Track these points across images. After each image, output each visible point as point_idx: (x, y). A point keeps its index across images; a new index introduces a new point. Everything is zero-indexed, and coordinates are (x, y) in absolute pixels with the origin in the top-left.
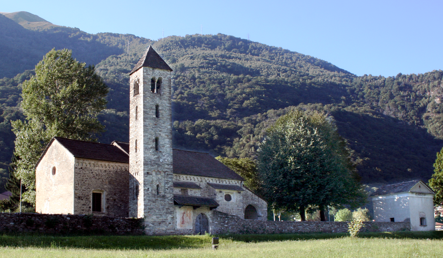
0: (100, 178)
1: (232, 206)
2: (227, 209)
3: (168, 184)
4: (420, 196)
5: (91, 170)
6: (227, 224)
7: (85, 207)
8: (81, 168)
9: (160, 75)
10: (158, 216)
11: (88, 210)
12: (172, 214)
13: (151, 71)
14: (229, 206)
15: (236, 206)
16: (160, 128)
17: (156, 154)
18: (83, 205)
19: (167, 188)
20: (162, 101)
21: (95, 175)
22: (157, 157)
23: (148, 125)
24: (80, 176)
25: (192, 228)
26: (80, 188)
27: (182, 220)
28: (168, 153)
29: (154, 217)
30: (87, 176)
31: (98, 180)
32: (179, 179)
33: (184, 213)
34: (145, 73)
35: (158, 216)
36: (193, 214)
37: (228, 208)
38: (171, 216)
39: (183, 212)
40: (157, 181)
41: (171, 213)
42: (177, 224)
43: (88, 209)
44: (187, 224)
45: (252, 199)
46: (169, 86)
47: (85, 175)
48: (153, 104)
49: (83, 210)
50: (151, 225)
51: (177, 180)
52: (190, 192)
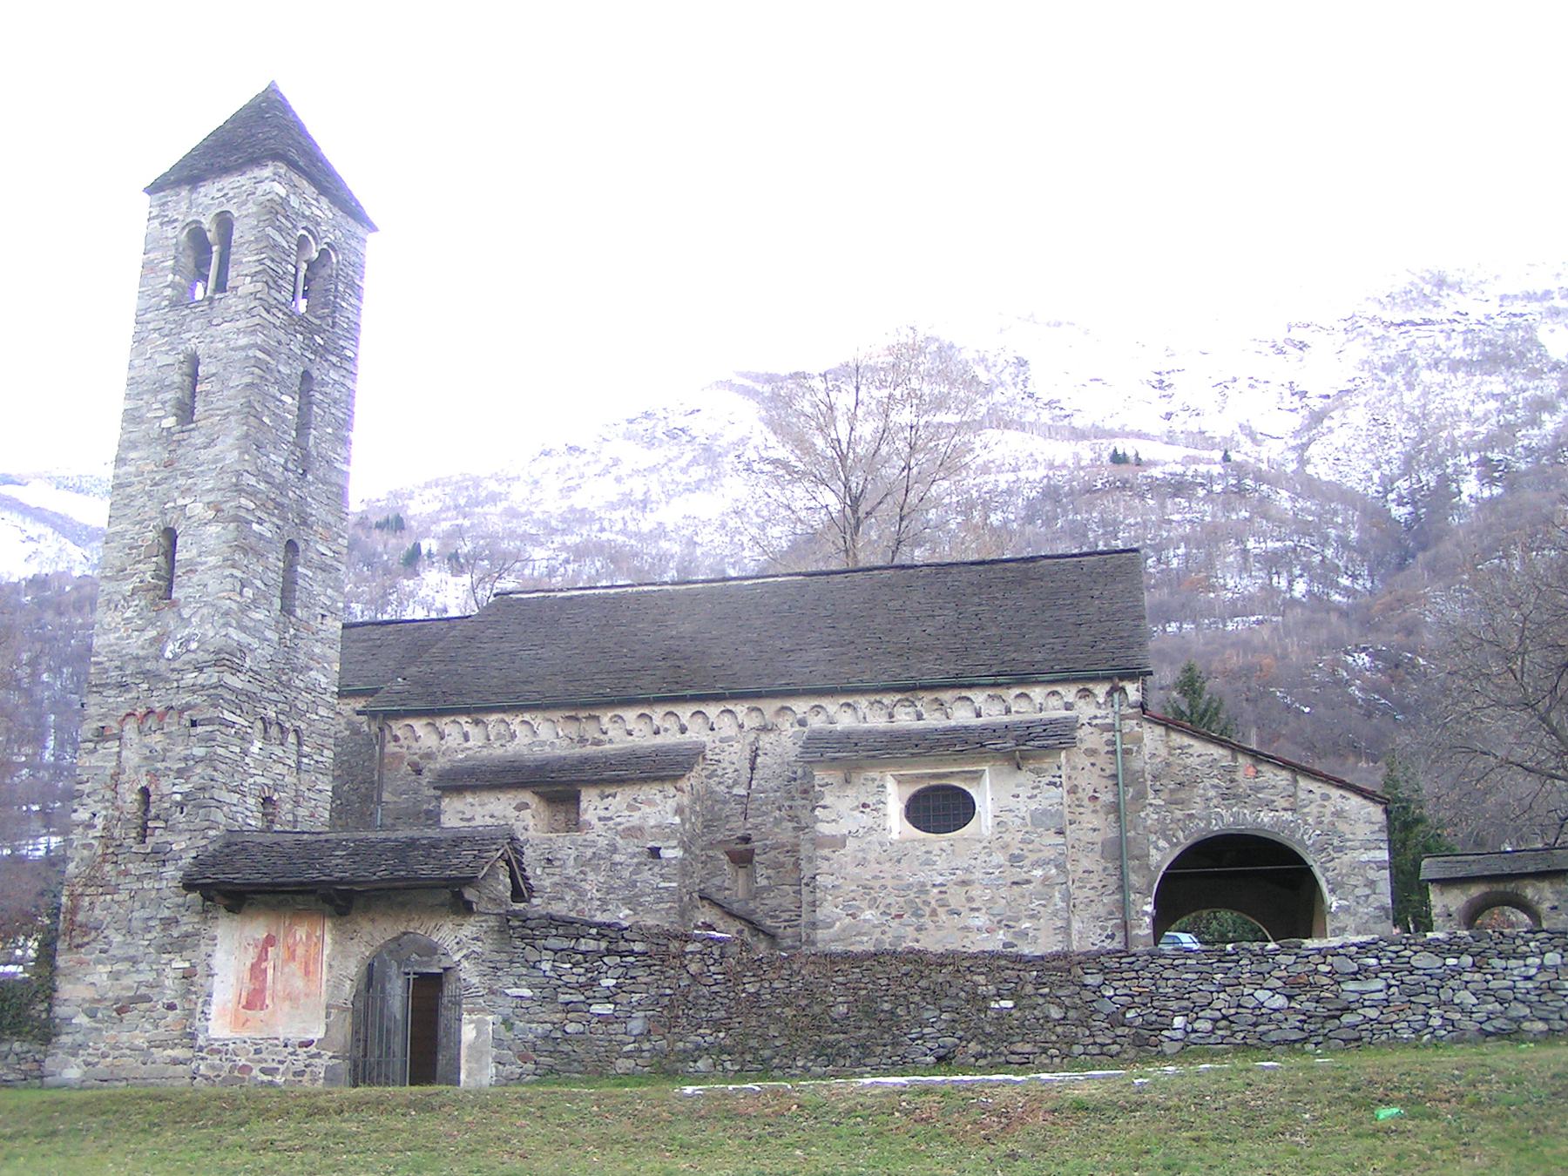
2: (909, 886)
10: (117, 967)
12: (187, 954)
15: (999, 858)
16: (189, 475)
22: (154, 633)
25: (318, 1033)
27: (248, 986)
32: (597, 735)
33: (270, 941)
35: (117, 967)
36: (335, 942)
37: (921, 877)
39: (262, 935)
41: (180, 945)
42: (213, 1011)
44: (286, 1006)
51: (582, 740)
52: (596, 801)
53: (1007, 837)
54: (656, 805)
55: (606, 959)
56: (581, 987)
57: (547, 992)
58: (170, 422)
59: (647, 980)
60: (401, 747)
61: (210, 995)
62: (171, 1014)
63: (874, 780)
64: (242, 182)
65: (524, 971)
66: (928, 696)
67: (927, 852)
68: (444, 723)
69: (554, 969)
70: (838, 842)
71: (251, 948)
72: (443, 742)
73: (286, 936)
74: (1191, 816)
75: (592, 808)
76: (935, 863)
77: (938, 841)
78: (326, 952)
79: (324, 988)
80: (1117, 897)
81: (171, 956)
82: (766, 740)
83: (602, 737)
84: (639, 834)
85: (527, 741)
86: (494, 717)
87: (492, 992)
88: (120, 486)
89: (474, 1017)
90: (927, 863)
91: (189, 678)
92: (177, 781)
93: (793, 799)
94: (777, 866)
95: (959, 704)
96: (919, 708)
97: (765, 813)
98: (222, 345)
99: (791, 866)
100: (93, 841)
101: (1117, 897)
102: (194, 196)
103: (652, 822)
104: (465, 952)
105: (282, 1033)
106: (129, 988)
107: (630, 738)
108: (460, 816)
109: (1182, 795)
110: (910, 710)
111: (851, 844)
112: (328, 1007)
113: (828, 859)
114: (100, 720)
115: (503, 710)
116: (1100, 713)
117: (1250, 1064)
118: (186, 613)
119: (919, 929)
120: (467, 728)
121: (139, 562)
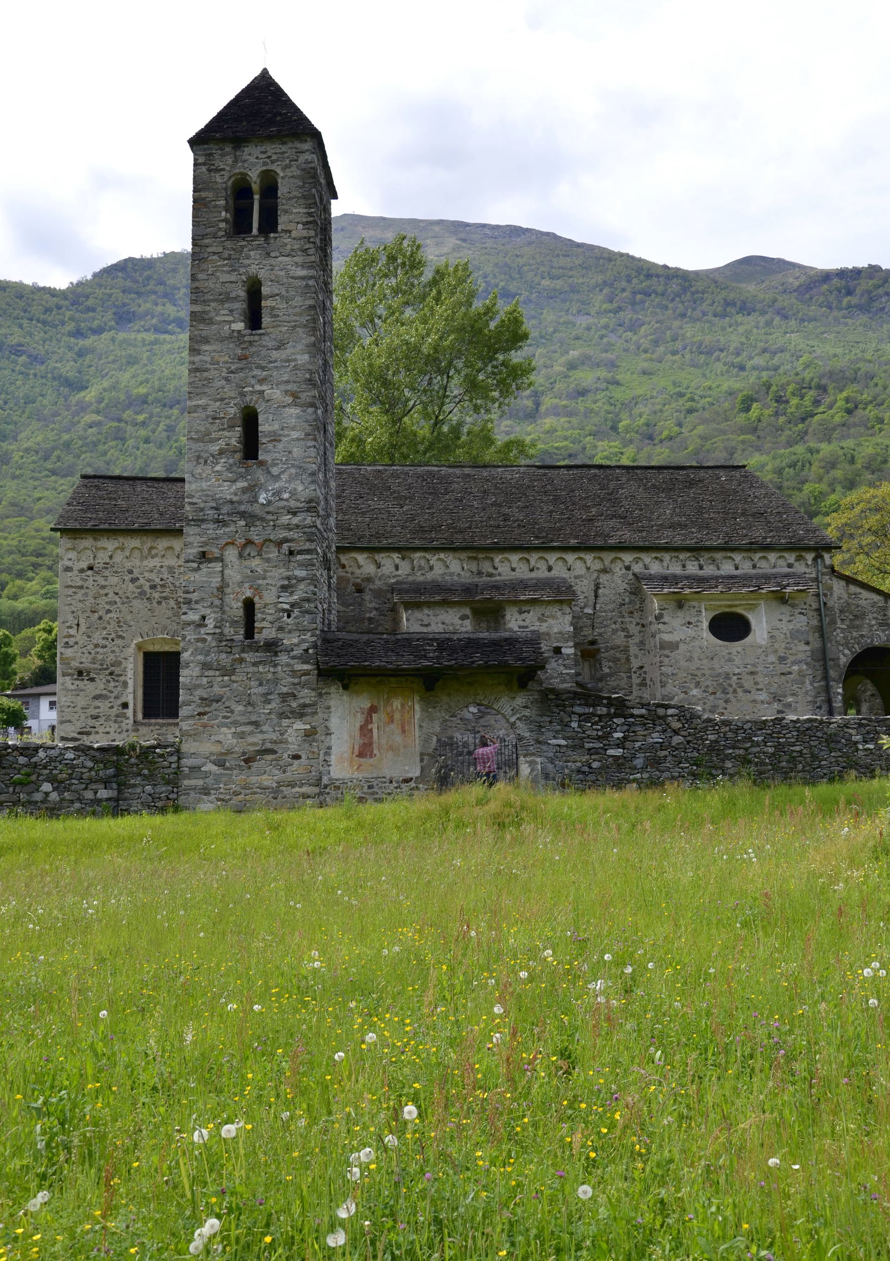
0: (165, 598)
1: (748, 661)
2: (719, 675)
3: (292, 593)
5: (130, 572)
6: (621, 744)
7: (104, 706)
8: (91, 568)
9: (265, 164)
10: (239, 729)
11: (117, 716)
12: (307, 719)
13: (228, 154)
14: (730, 660)
15: (772, 658)
16: (263, 368)
17: (242, 476)
18: (96, 697)
19: (284, 610)
20: (272, 261)
21: (146, 588)
22: (245, 484)
23: (208, 366)
24: (86, 595)
26: (81, 638)
27: (359, 741)
28: (293, 466)
29: (227, 736)
30: (111, 595)
31: (159, 603)
32: (491, 570)
33: (373, 709)
34: (204, 169)
35: (239, 729)
36: (423, 710)
37: (726, 669)
38: (299, 725)
39: (367, 705)
40: (247, 585)
42: (333, 759)
43: (115, 711)
44: (390, 754)
46: (304, 197)
47: (103, 592)
48: (233, 279)
49: (96, 717)
51: (480, 573)
52: (516, 615)
53: (776, 645)
54: (557, 618)
55: (615, 720)
56: (599, 738)
57: (577, 742)
58: (240, 326)
59: (645, 733)
60: (347, 572)
61: (329, 748)
62: (296, 762)
63: (694, 607)
64: (284, 150)
65: (559, 727)
66: (707, 555)
67: (729, 654)
68: (380, 557)
69: (580, 726)
70: (674, 646)
71: (359, 714)
72: (379, 570)
73: (385, 706)
74: (862, 636)
75: (514, 619)
76: (734, 660)
77: (737, 646)
78: (417, 716)
79: (417, 741)
80: (822, 683)
81: (293, 720)
82: (604, 578)
83: (494, 571)
84: (547, 638)
85: (440, 572)
86: (418, 555)
87: (538, 742)
88: (197, 370)
89: (528, 759)
90: (730, 660)
91: (285, 519)
92: (282, 594)
93: (623, 617)
95: (724, 561)
96: (702, 562)
97: (606, 626)
98: (282, 273)
99: (623, 661)
100: (205, 636)
101: (822, 683)
102: (238, 153)
103: (556, 630)
104: (518, 716)
105: (388, 773)
106: (253, 744)
107: (513, 573)
108: (420, 623)
109: (857, 623)
110: (696, 563)
111: (682, 647)
112: (422, 754)
113: (668, 657)
114: (201, 547)
115: (425, 549)
116: (808, 570)
118: (275, 471)
119: (727, 701)
120: (397, 561)
121: (224, 430)
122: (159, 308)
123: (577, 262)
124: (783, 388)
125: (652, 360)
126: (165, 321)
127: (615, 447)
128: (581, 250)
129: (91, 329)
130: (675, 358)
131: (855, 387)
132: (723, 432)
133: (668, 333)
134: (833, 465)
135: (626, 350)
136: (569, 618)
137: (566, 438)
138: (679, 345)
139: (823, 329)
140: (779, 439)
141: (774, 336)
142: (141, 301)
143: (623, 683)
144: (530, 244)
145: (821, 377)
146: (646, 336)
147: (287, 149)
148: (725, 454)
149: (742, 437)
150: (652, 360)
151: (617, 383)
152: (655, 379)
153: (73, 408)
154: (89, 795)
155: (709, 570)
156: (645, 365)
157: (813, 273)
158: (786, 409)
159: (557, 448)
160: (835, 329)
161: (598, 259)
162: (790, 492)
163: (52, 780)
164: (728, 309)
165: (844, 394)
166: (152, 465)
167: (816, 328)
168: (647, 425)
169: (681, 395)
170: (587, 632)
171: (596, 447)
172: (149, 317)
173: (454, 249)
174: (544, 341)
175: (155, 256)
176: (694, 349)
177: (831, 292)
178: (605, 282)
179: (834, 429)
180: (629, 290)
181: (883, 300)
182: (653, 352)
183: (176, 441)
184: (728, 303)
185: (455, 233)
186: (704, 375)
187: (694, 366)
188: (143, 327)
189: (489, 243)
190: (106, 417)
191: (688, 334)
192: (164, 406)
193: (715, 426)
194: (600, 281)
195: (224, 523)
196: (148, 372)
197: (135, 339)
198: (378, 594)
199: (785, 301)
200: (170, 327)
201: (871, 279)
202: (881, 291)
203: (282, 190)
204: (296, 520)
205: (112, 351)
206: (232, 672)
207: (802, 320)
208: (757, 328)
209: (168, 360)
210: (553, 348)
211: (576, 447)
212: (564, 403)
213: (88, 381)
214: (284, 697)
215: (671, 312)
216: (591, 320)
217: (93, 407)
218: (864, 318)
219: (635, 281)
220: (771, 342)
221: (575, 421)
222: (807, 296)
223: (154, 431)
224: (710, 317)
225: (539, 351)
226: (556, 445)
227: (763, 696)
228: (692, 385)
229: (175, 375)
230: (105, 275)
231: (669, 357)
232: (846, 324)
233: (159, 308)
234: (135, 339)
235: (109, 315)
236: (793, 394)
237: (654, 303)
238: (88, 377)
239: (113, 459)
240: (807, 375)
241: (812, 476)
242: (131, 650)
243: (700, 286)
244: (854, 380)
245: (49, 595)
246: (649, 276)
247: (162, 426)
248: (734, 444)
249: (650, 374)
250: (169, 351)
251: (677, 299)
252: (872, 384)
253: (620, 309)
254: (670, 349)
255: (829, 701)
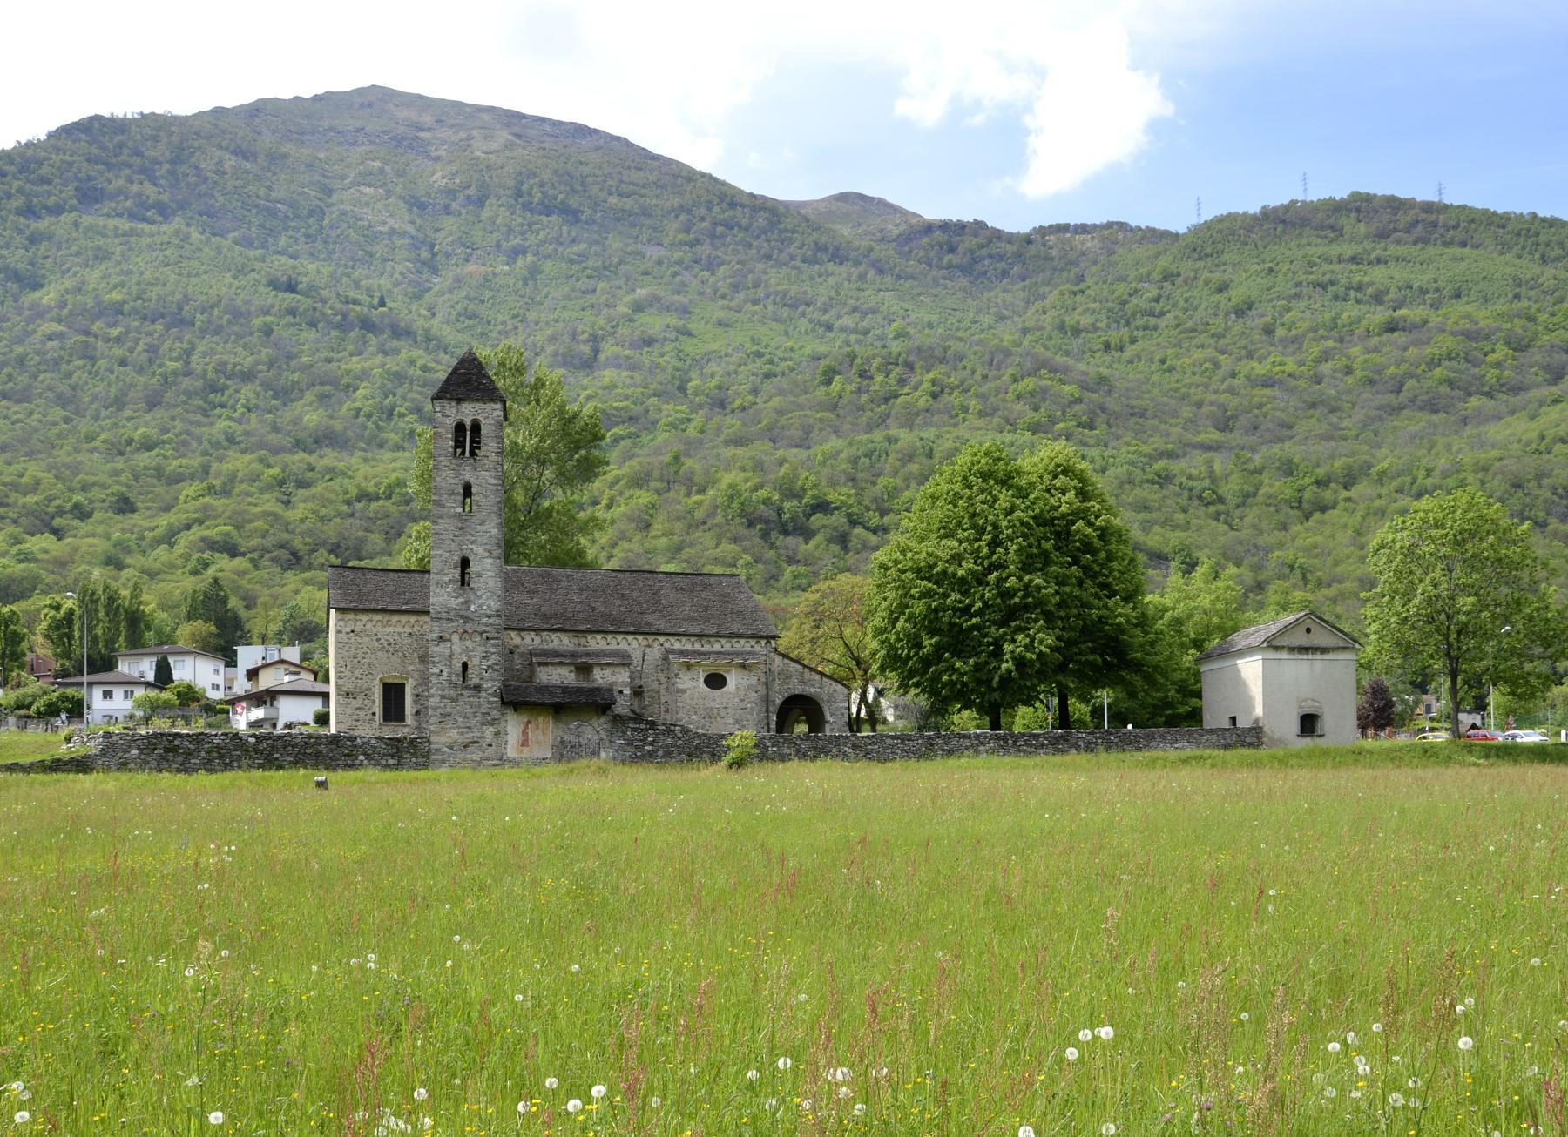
4: (1305, 657)
6: (652, 744)
7: (362, 714)
15: (737, 700)
26: (348, 674)
27: (522, 738)
29: (454, 734)
33: (529, 722)
38: (492, 729)
42: (509, 747)
43: (369, 717)
45: (802, 682)
50: (445, 749)
68: (523, 634)
70: (684, 691)
91: (485, 620)
94: (652, 697)
115: (549, 630)
117: (1350, 460)
118: (479, 593)
122: (135, 188)
123: (651, 178)
124: (868, 360)
125: (730, 308)
126: (143, 204)
127: (682, 412)
128: (656, 163)
129: (45, 207)
130: (756, 308)
131: (943, 368)
132: (800, 407)
133: (750, 276)
134: (909, 457)
135: (701, 293)
136: (628, 674)
137: (627, 398)
138: (761, 293)
139: (919, 290)
140: (860, 420)
141: (866, 293)
142: (111, 175)
143: (656, 711)
144: (597, 149)
145: (908, 353)
146: (725, 278)
147: (488, 407)
148: (800, 433)
149: (819, 415)
150: (730, 308)
151: (689, 334)
152: (731, 331)
153: (27, 313)
154: (384, 762)
155: (707, 648)
156: (720, 314)
157: (914, 221)
158: (869, 386)
159: (616, 409)
160: (933, 291)
161: (675, 176)
162: (864, 485)
163: (364, 754)
164: (819, 255)
165: (931, 375)
166: (131, 394)
167: (912, 288)
168: (719, 388)
169: (759, 355)
170: (637, 681)
171: (660, 410)
172: (122, 198)
173: (506, 146)
174: (607, 273)
175: (129, 116)
176: (778, 300)
177: (932, 247)
178: (682, 206)
179: (917, 414)
180: (708, 220)
181: (986, 263)
182: (732, 299)
183: (160, 366)
184: (820, 248)
185: (508, 125)
186: (787, 333)
187: (776, 320)
188: (114, 210)
189: (549, 143)
190: (70, 328)
191: (773, 281)
192: (145, 318)
193: (792, 398)
194: (676, 205)
195: (452, 621)
196: (122, 273)
197: (105, 226)
198: (522, 655)
199: (885, 252)
200: (149, 214)
201: (976, 236)
202: (984, 252)
203: (483, 431)
204: (490, 621)
205: (75, 240)
206: (457, 701)
207: (899, 277)
208: (849, 281)
209: (148, 259)
210: (617, 283)
211: (638, 409)
212: (627, 352)
213: (44, 277)
214: (484, 714)
215: (754, 251)
216: (663, 253)
217: (53, 313)
218: (963, 282)
219: (716, 209)
220: (862, 300)
221: (638, 376)
222: (906, 249)
223: (131, 351)
224: (798, 263)
225: (601, 285)
226: (615, 404)
227: (731, 720)
228: (772, 343)
229: (158, 279)
230: (64, 135)
231: (749, 306)
232: (945, 287)
233: (135, 188)
234: (105, 226)
235: (70, 190)
236: (878, 369)
237: (737, 239)
238: (43, 272)
239: (81, 382)
240: (895, 347)
241: (888, 468)
242: (377, 681)
243: (789, 223)
244: (943, 360)
245: (22, 557)
246: (732, 205)
247: (141, 346)
248: (811, 421)
249: (727, 325)
250: (149, 246)
251: (763, 237)
252: (960, 366)
253: (697, 242)
254: (751, 296)
255: (768, 725)
